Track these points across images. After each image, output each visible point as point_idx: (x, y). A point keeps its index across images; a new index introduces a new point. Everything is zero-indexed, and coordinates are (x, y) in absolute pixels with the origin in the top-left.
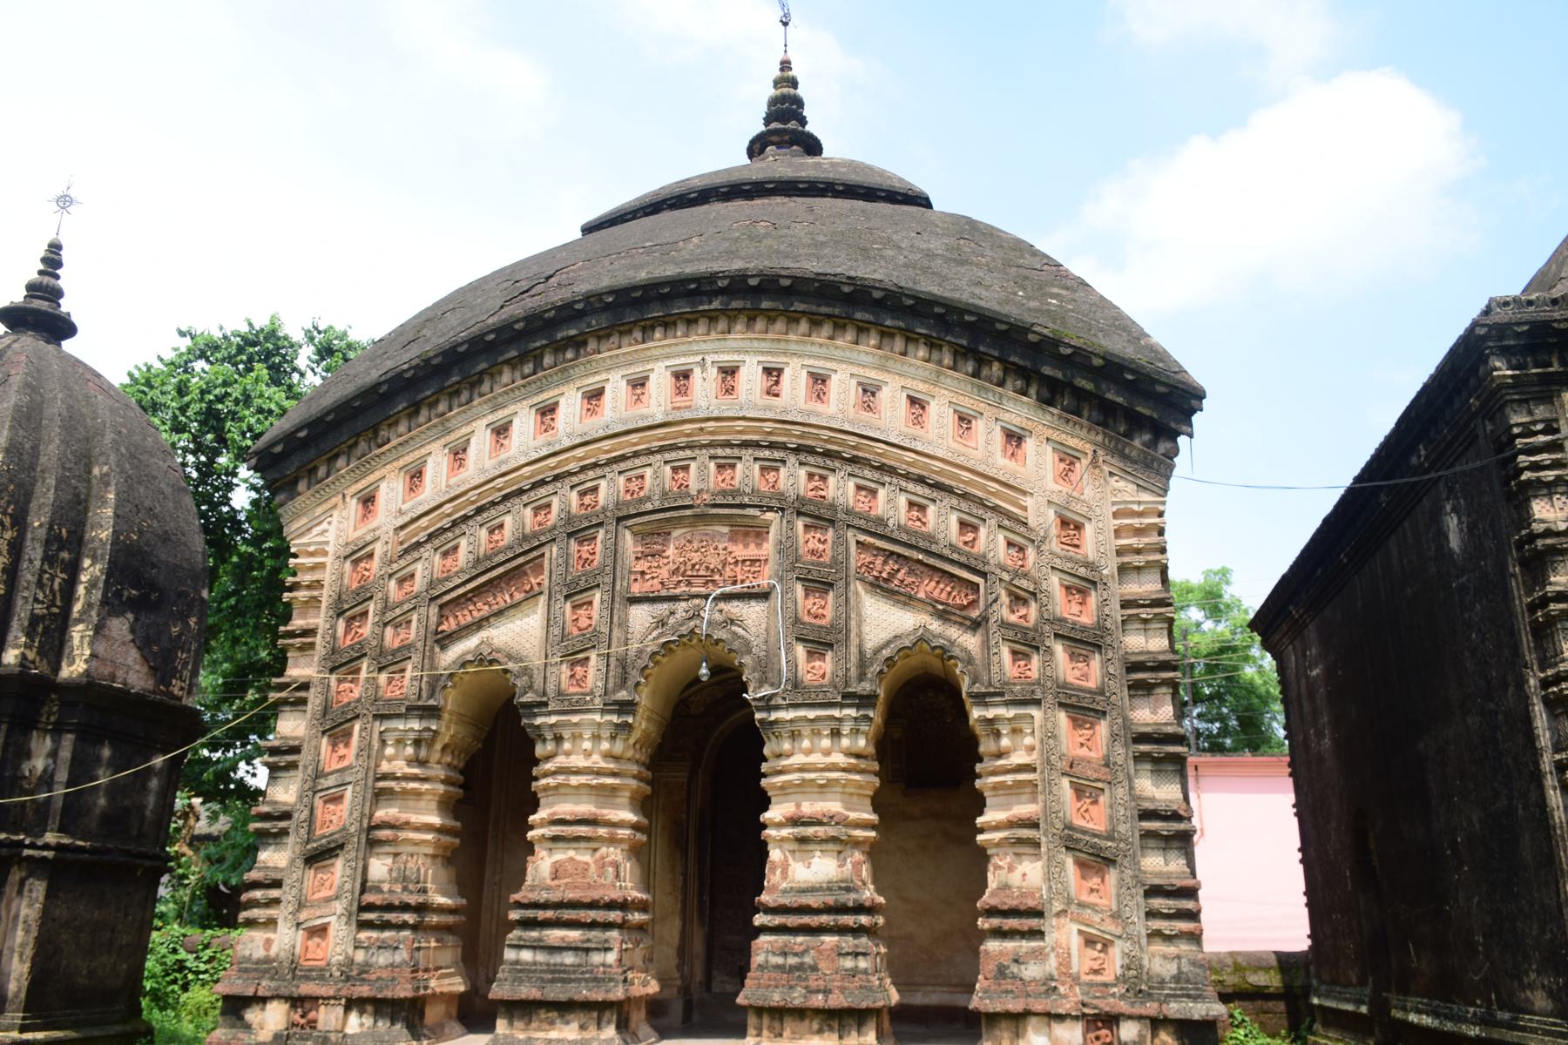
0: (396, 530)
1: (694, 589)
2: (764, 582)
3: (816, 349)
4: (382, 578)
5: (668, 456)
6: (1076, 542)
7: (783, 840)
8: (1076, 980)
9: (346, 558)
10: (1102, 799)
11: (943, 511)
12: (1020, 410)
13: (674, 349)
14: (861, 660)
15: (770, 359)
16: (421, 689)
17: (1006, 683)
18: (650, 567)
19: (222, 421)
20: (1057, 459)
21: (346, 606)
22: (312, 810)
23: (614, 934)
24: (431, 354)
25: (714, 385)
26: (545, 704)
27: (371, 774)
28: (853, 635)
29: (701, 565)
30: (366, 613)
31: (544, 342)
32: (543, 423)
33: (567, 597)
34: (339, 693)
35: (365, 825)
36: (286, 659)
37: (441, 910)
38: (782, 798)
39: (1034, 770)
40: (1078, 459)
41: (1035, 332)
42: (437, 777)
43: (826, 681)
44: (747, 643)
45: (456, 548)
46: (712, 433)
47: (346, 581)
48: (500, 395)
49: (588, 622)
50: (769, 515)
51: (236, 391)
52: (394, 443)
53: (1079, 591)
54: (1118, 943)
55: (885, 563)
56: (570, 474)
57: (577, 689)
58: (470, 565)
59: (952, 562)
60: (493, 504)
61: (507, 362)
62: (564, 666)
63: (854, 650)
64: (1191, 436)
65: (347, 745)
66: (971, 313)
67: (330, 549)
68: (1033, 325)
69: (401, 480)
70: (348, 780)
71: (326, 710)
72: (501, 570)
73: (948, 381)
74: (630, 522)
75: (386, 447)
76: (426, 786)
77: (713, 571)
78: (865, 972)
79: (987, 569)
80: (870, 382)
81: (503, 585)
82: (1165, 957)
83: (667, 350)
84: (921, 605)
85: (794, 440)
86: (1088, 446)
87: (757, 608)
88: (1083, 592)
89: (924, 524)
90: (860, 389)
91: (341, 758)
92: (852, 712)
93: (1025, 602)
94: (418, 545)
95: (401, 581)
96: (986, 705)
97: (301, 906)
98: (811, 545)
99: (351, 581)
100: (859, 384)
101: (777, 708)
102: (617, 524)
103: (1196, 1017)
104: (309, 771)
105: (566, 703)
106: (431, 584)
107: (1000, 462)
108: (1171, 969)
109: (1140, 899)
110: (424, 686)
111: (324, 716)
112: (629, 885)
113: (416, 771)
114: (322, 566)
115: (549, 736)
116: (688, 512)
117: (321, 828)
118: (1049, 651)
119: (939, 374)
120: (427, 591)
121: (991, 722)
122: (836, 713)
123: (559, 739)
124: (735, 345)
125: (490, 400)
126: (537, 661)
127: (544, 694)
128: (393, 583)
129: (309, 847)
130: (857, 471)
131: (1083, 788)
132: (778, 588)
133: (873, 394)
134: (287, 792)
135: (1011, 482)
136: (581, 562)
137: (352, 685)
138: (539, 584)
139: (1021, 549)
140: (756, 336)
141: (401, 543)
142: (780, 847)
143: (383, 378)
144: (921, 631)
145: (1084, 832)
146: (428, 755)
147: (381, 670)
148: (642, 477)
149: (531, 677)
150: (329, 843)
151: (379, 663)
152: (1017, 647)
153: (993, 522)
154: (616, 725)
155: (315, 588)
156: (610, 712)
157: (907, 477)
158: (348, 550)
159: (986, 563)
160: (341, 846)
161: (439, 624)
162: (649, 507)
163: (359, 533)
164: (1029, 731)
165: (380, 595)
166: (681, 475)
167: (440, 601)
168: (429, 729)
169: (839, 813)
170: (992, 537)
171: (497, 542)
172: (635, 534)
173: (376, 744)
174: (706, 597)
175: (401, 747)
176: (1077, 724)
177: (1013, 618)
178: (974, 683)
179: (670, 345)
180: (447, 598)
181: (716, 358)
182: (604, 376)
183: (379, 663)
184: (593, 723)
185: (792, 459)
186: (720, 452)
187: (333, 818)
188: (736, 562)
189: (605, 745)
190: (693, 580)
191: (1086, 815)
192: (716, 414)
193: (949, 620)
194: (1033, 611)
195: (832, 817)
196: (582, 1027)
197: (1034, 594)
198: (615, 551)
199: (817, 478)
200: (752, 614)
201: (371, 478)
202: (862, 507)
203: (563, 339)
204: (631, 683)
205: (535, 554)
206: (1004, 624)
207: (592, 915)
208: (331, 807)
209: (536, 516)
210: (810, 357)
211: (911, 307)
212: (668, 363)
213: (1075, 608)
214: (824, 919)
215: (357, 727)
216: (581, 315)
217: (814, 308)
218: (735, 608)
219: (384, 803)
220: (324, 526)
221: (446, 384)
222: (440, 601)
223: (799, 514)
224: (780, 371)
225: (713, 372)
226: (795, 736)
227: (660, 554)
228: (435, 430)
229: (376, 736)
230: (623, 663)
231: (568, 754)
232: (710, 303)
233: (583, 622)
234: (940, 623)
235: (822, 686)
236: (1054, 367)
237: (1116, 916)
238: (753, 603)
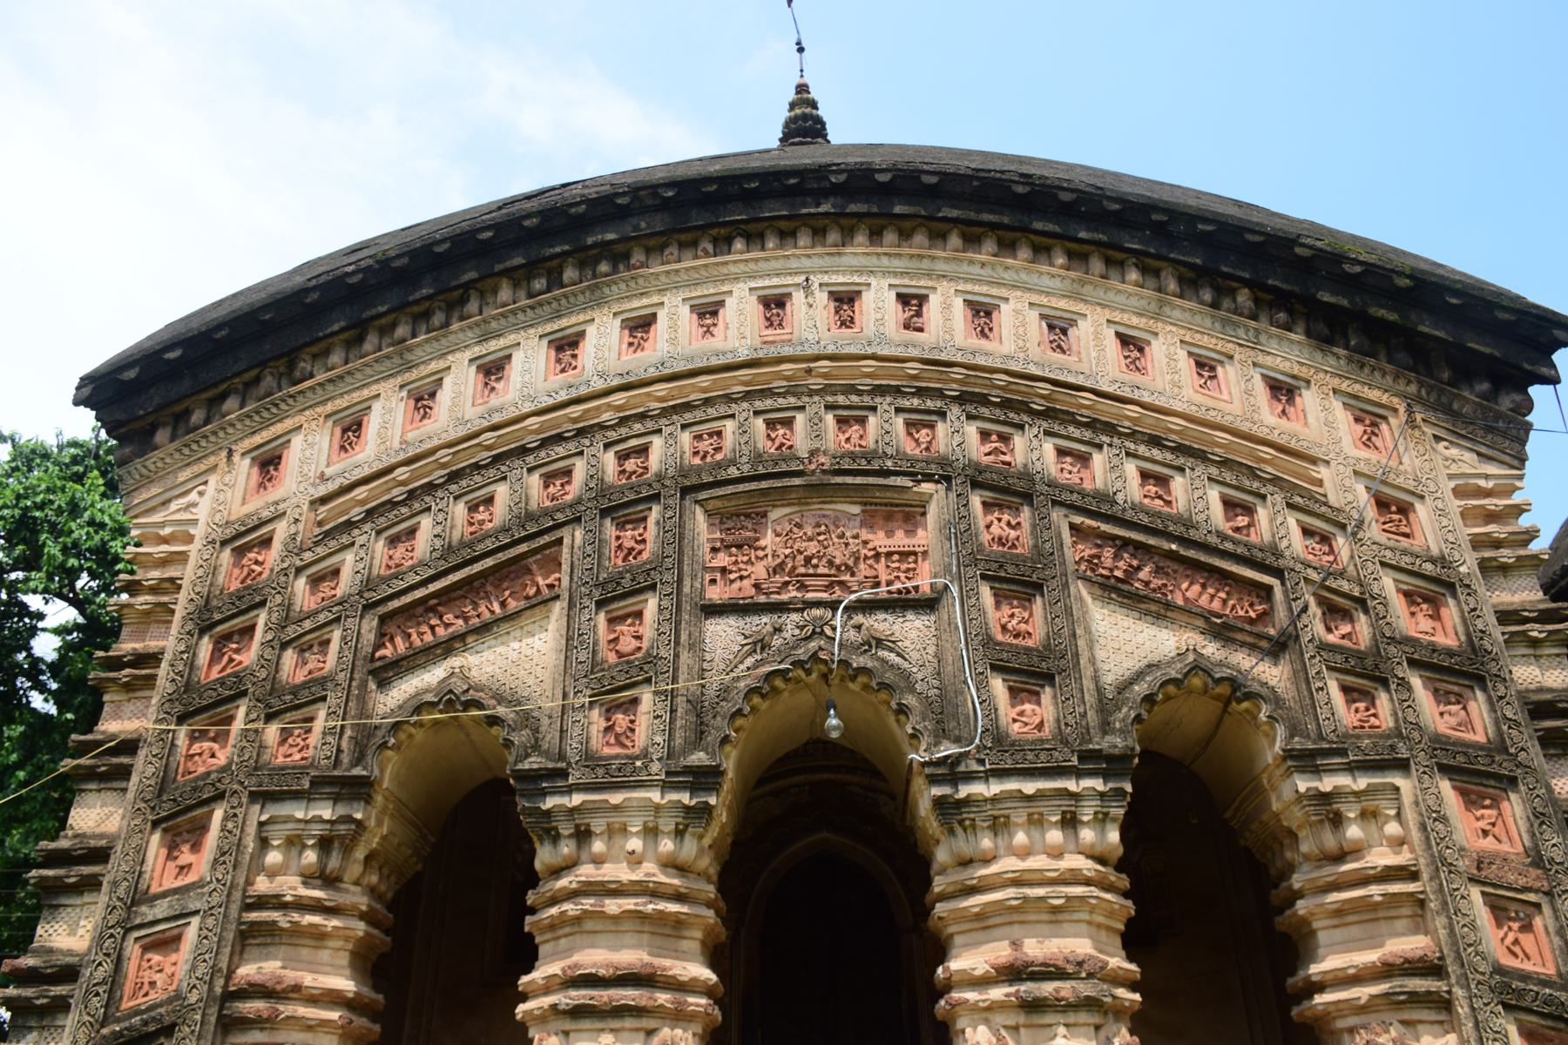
0: (312, 503)
1: (810, 595)
2: (924, 581)
3: (976, 269)
4: (285, 573)
5: (759, 405)
6: (1407, 530)
7: (993, 1007)
9: (224, 543)
10: (1538, 922)
11: (1197, 483)
13: (763, 265)
14: (1100, 701)
15: (906, 281)
16: (339, 751)
17: (1346, 736)
18: (736, 562)
19: (36, 533)
20: (1351, 418)
21: (217, 617)
22: (119, 962)
24: (392, 253)
25: (825, 313)
26: (563, 774)
27: (237, 895)
29: (820, 558)
30: (251, 629)
31: (566, 248)
32: (559, 361)
33: (600, 604)
34: (190, 757)
35: (218, 990)
36: (99, 706)
38: (981, 935)
39: (1414, 876)
40: (1384, 418)
41: (1303, 245)
42: (354, 907)
43: (1047, 732)
44: (906, 676)
45: (412, 532)
47: (220, 579)
48: (494, 318)
49: (635, 644)
50: (927, 487)
51: (60, 500)
52: (321, 377)
53: (1426, 599)
56: (602, 427)
57: (617, 750)
58: (435, 555)
59: (1224, 554)
60: (477, 467)
61: (507, 273)
62: (595, 713)
64: (1554, 381)
65: (196, 847)
66: (1205, 220)
67: (198, 532)
68: (1299, 236)
69: (327, 432)
70: (192, 907)
71: (164, 782)
72: (489, 562)
73: (1177, 313)
74: (703, 495)
75: (307, 384)
76: (335, 922)
77: (838, 568)
80: (1059, 314)
81: (489, 588)
83: (752, 266)
84: (1185, 618)
85: (955, 386)
86: (1395, 400)
87: (918, 623)
88: (1434, 602)
89: (1168, 503)
90: (1044, 325)
91: (184, 869)
92: (1097, 784)
93: (1347, 616)
94: (349, 525)
95: (315, 581)
96: (1317, 771)
98: (995, 530)
99: (229, 575)
101: (970, 777)
102: (682, 498)
104: (121, 892)
105: (600, 772)
106: (369, 584)
107: (1267, 417)
110: (344, 745)
111: (160, 795)
114: (182, 558)
115: (566, 829)
116: (797, 481)
117: (134, 996)
118: (1404, 684)
119: (1162, 304)
120: (360, 593)
121: (1324, 798)
122: (1071, 785)
123: (583, 835)
124: (854, 261)
125: (477, 324)
126: (551, 704)
127: (562, 756)
128: (381, 543)
129: (105, 1031)
130: (1057, 428)
131: (1503, 903)
132: (955, 590)
133: (1064, 332)
134: (72, 933)
135: (1293, 444)
136: (621, 555)
137: (216, 746)
138: (551, 586)
139: (1325, 539)
140: (885, 250)
141: (320, 524)
142: (987, 1022)
143: (314, 282)
144: (1191, 657)
146: (342, 868)
147: (269, 718)
148: (719, 434)
149: (537, 731)
150: (145, 1023)
151: (268, 706)
152: (1350, 679)
153: (1278, 498)
154: (687, 809)
155: (165, 592)
156: (677, 787)
158: (229, 532)
159: (1278, 554)
161: (379, 645)
162: (733, 472)
163: (250, 508)
164: (1392, 812)
165: (278, 599)
166: (781, 432)
167: (382, 610)
168: (348, 819)
169: (1092, 957)
170: (1280, 519)
171: (482, 522)
172: (709, 514)
173: (250, 844)
174: (833, 606)
175: (294, 852)
176: (1471, 800)
177: (1331, 638)
178: (1292, 736)
179: (756, 260)
180: (396, 604)
181: (826, 279)
182: (655, 299)
183: (268, 706)
185: (955, 411)
186: (841, 399)
187: (158, 977)
188: (877, 556)
189: (667, 845)
190: (809, 582)
191: (1517, 949)
192: (831, 350)
193: (1233, 641)
194: (1363, 630)
195: (1080, 964)
197: (1361, 602)
198: (677, 537)
199: (994, 437)
200: (911, 631)
201: (278, 428)
203: (595, 245)
204: (712, 738)
205: (547, 539)
206: (1323, 647)
208: (156, 958)
209: (546, 486)
210: (966, 280)
212: (753, 284)
213: (1425, 624)
215: (218, 814)
216: (622, 214)
217: (972, 215)
218: (881, 623)
219: (255, 951)
220: (193, 496)
221: (411, 298)
222: (382, 610)
223: (975, 485)
224: (922, 299)
225: (822, 297)
226: (999, 826)
227: (752, 544)
228: (388, 363)
229: (251, 829)
230: (697, 707)
231: (598, 861)
232: (818, 205)
233: (627, 644)
234: (1218, 645)
235: (1042, 741)
236: (1334, 293)
238: (910, 616)
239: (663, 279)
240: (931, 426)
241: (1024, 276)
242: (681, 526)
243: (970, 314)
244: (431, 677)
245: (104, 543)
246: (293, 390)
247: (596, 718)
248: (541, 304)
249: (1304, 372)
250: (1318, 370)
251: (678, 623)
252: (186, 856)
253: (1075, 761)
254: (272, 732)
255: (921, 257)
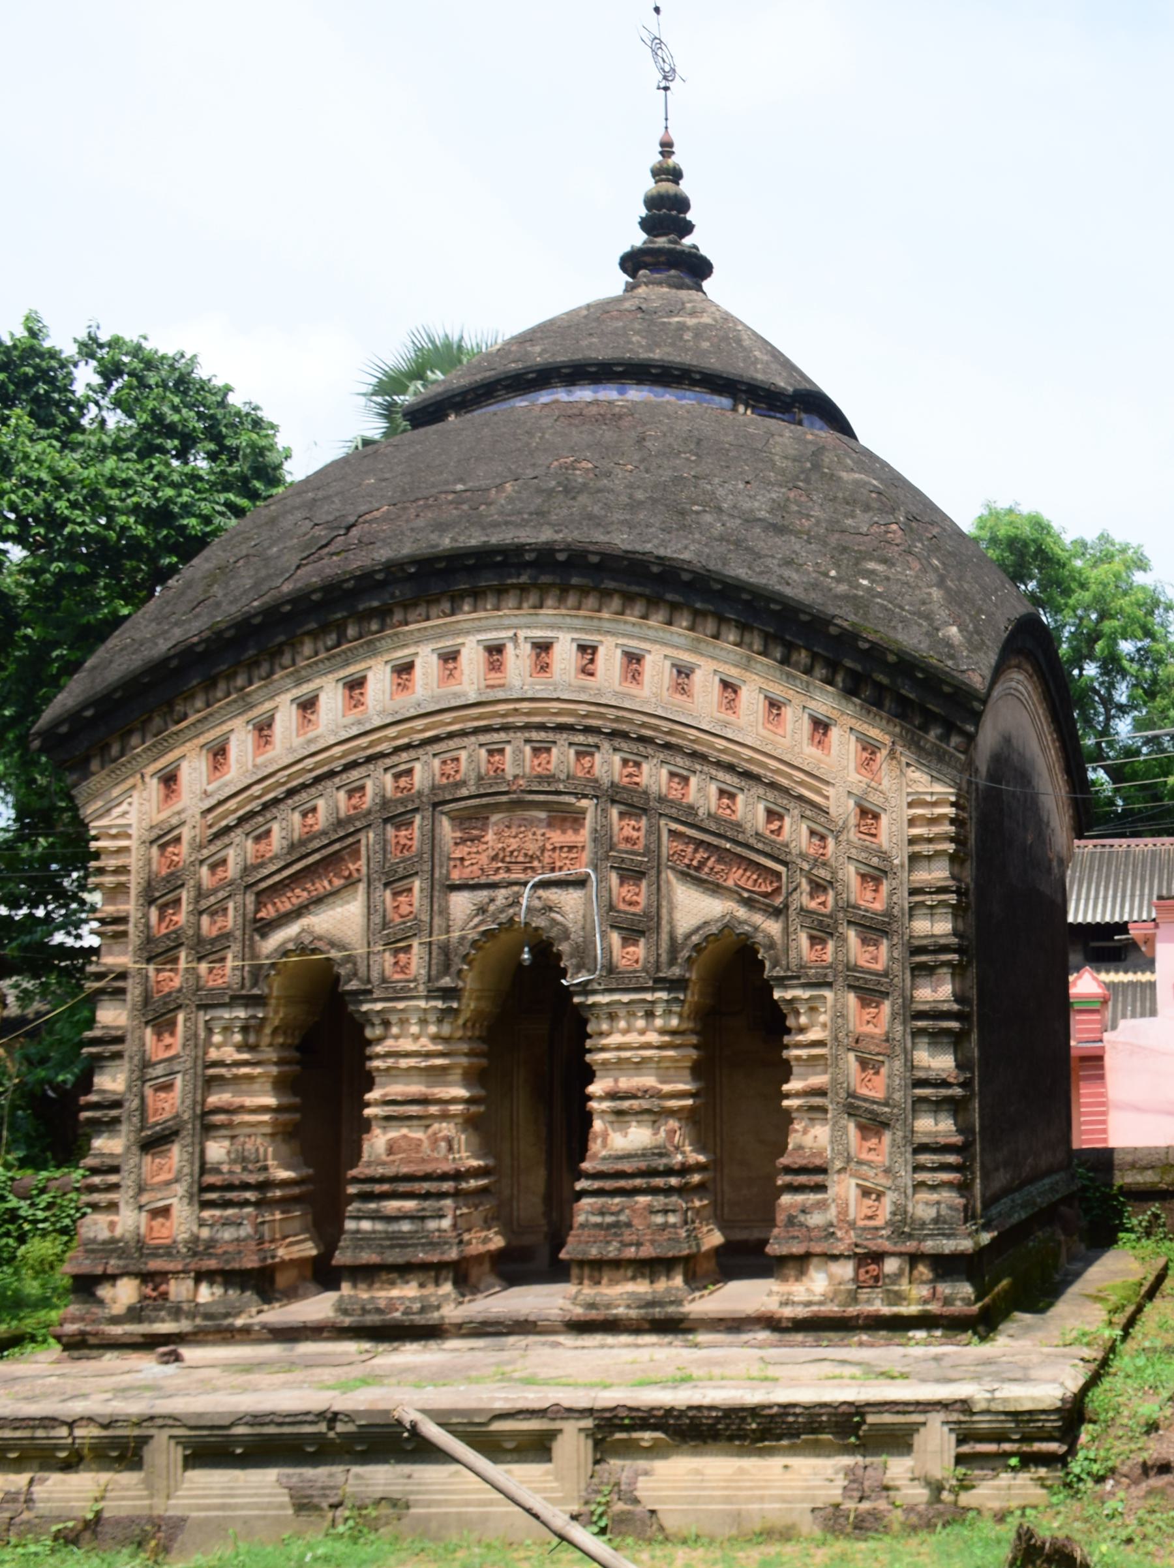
3: (629, 628)
6: (873, 831)
8: (852, 1225)
9: (152, 842)
11: (751, 800)
12: (825, 702)
13: (484, 623)
21: (157, 894)
23: (448, 1202)
24: (223, 626)
26: (370, 992)
27: (200, 1062)
28: (664, 922)
30: (178, 901)
33: (386, 885)
34: (158, 982)
37: (284, 1184)
45: (268, 833)
46: (528, 714)
47: (154, 867)
48: (304, 668)
50: (584, 803)
52: (192, 719)
54: (889, 1193)
55: (696, 851)
61: (309, 633)
63: (665, 937)
65: (172, 1034)
68: (834, 617)
70: (177, 1068)
74: (447, 808)
78: (674, 1226)
79: (788, 858)
82: (927, 1203)
83: (477, 623)
91: (168, 1047)
92: (663, 995)
94: (228, 829)
95: (213, 867)
97: (141, 1189)
100: (673, 665)
101: (594, 992)
103: (947, 1251)
106: (246, 870)
108: (932, 1213)
109: (909, 1156)
110: (246, 974)
112: (465, 1154)
113: (245, 1056)
115: (377, 1021)
116: (504, 798)
122: (648, 996)
123: (386, 1024)
124: (547, 620)
125: (292, 673)
126: (361, 951)
127: (369, 981)
132: (593, 876)
141: (210, 826)
145: (865, 1100)
148: (457, 759)
157: (719, 764)
160: (176, 1133)
161: (257, 911)
162: (464, 792)
163: (164, 815)
172: (452, 819)
173: (202, 1034)
176: (864, 1003)
177: (813, 905)
182: (412, 650)
184: (418, 1008)
185: (606, 745)
189: (433, 1029)
190: (513, 867)
192: (529, 695)
196: (422, 1285)
197: (831, 883)
198: (432, 838)
200: (570, 902)
202: (674, 795)
207: (426, 1186)
209: (350, 798)
210: (624, 635)
211: (719, 591)
212: (480, 637)
213: (869, 895)
214: (638, 1182)
218: (553, 895)
220: (124, 807)
223: (613, 802)
224: (594, 649)
225: (527, 648)
226: (612, 1017)
228: (235, 706)
229: (201, 1025)
231: (397, 1037)
233: (405, 909)
237: (887, 1171)
238: (571, 890)
239: (417, 634)
240: (592, 754)
241: (661, 634)
242: (433, 830)
243: (625, 660)
244: (292, 930)
245: (48, 505)
246: (175, 728)
247: (389, 958)
248: (334, 656)
249: (834, 714)
250: (843, 713)
251: (432, 898)
252: (168, 1040)
253: (650, 984)
254: (203, 967)
255: (591, 618)
